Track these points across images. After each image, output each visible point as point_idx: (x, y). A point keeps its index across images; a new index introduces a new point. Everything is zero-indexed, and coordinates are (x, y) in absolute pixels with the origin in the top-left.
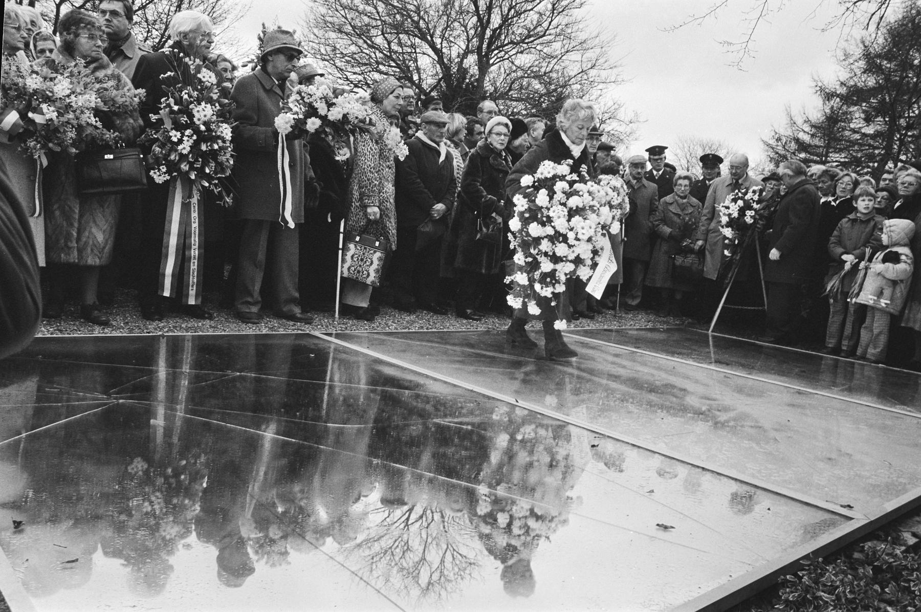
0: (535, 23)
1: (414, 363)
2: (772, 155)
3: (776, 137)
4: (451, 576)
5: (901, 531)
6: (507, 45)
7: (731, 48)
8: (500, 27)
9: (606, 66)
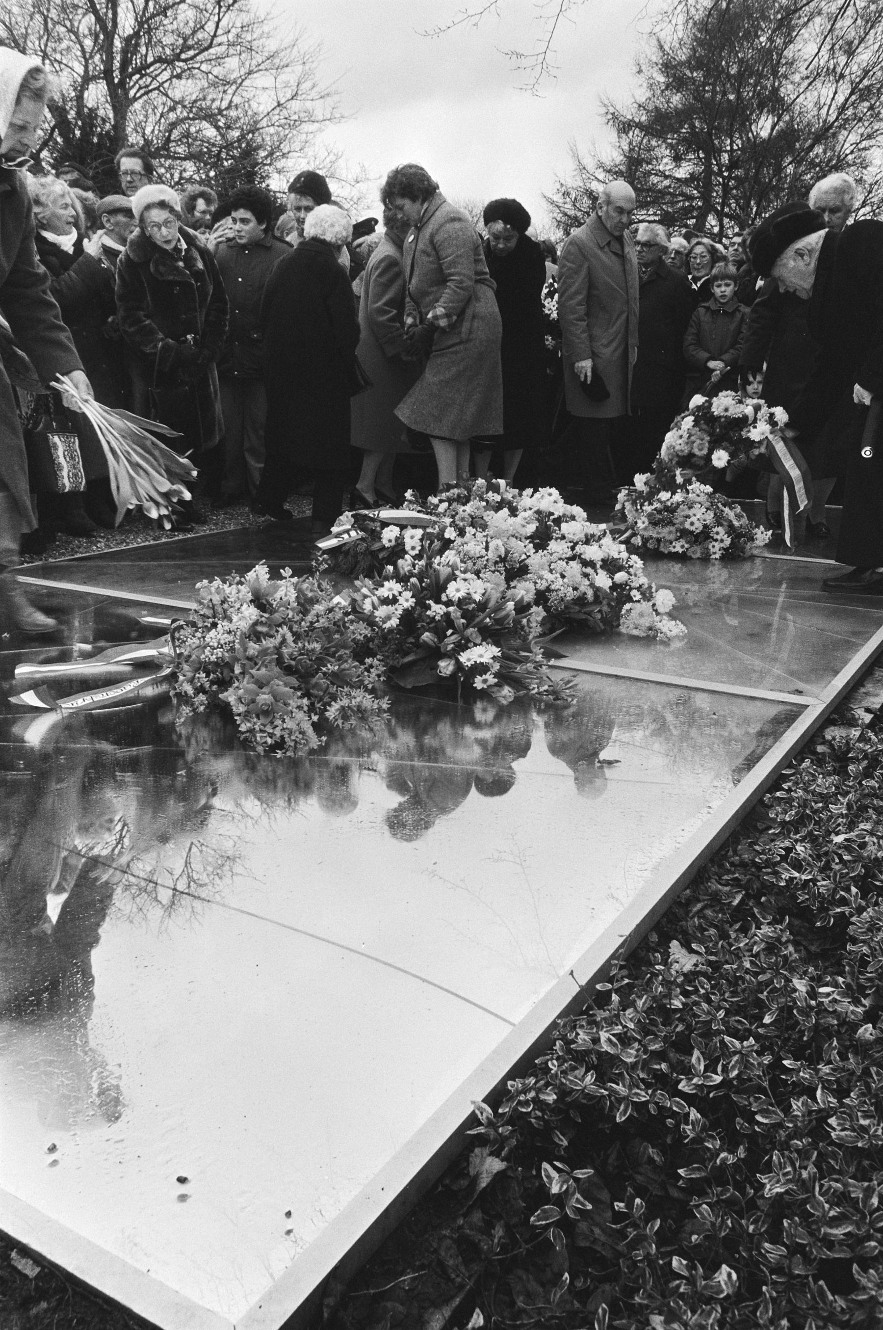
0: (191, 24)
1: (165, 594)
2: (559, 216)
3: (563, 189)
4: (204, 879)
5: (852, 709)
6: (152, 64)
7: (524, 62)
8: (136, 35)
9: (314, 94)
